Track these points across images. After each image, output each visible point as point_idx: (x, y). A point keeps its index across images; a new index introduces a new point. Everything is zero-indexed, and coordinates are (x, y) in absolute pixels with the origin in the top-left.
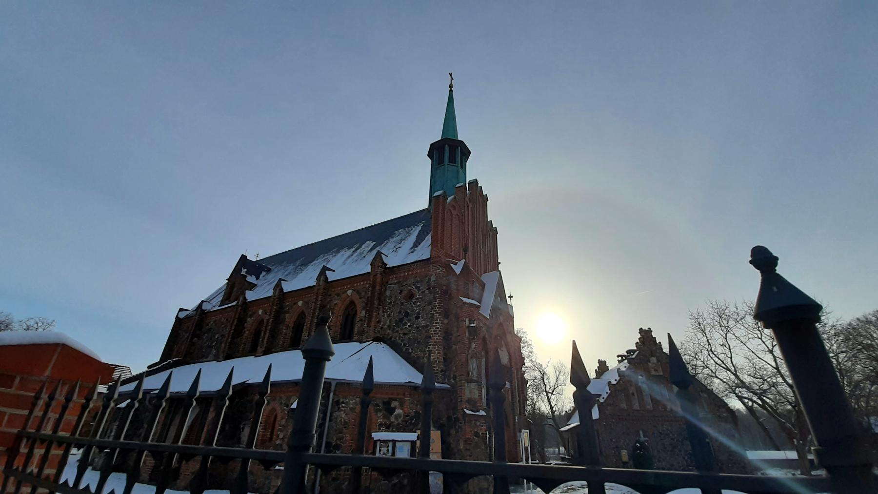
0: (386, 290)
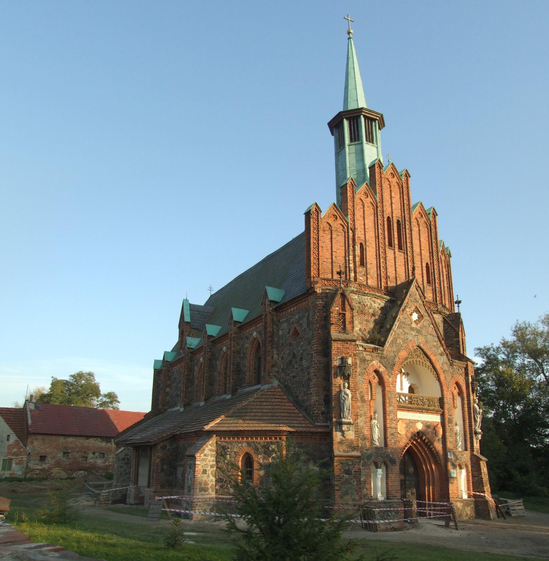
0: (278, 331)
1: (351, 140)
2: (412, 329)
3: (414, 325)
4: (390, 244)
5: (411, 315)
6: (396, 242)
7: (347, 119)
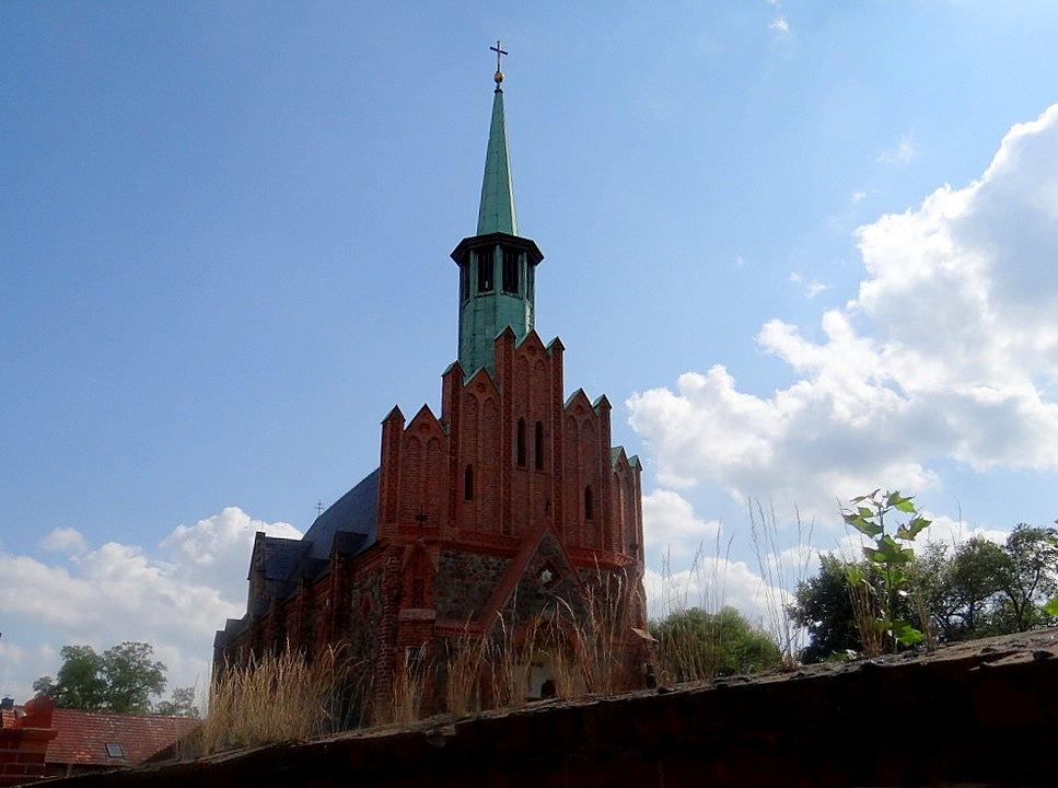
0: (350, 601)
1: (505, 288)
2: (539, 596)
3: (542, 590)
4: (522, 461)
5: (540, 573)
6: (533, 458)
7: (476, 251)
